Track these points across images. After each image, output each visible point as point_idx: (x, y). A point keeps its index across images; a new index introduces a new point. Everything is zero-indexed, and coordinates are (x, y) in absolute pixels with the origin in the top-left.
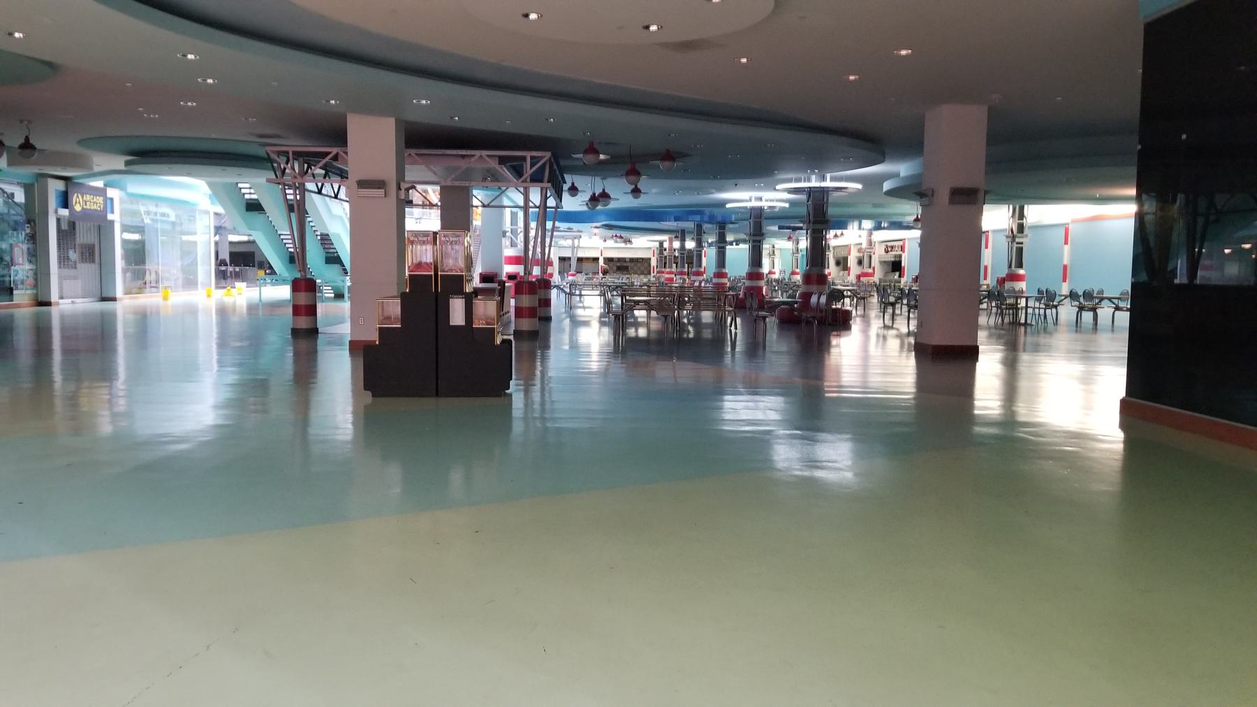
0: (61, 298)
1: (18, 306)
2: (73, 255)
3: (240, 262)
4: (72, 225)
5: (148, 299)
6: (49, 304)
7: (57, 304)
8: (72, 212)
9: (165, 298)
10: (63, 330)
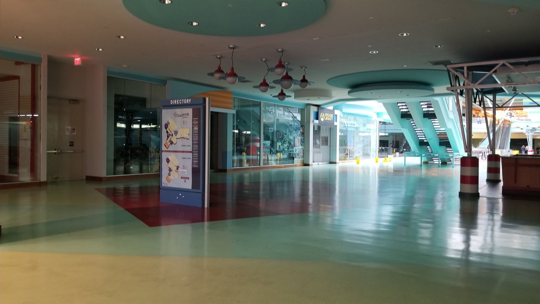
0: (314, 162)
1: (296, 166)
2: (318, 142)
3: (391, 144)
4: (319, 127)
5: (349, 164)
6: (308, 165)
7: (312, 165)
8: (320, 122)
9: (358, 163)
10: (315, 184)
